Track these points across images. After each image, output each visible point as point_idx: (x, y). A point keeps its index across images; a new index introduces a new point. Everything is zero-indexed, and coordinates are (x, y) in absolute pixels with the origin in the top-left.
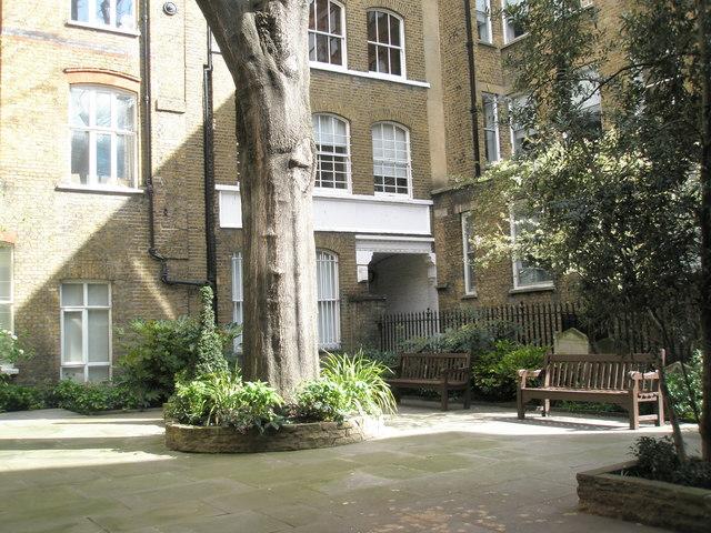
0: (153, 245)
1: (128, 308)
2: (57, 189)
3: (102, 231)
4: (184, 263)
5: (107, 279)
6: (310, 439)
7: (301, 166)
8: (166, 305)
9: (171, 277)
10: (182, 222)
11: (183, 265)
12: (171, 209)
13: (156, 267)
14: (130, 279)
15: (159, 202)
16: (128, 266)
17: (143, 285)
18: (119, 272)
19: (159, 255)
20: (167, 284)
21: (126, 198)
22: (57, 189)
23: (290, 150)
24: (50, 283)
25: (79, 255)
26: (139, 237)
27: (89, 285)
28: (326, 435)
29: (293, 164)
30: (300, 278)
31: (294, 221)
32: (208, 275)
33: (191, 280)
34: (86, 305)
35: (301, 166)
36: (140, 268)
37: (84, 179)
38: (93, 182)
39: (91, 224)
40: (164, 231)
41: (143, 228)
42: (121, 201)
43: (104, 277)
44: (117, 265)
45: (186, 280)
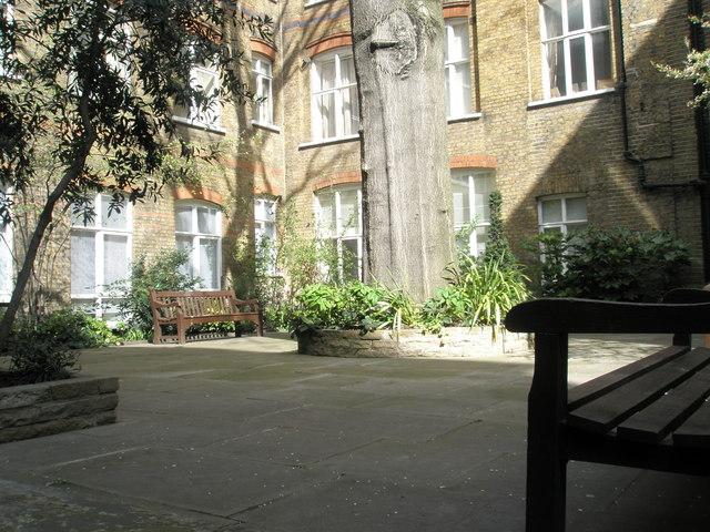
0: (627, 147)
1: (603, 220)
2: (530, 109)
3: (574, 141)
4: (667, 161)
5: (581, 191)
6: (332, 346)
7: (384, 46)
8: (647, 214)
9: (649, 181)
10: (664, 114)
11: (667, 165)
12: (649, 101)
13: (632, 171)
14: (604, 188)
15: (634, 96)
16: (602, 174)
17: (619, 193)
18: (592, 182)
19: (637, 157)
20: (649, 190)
21: (595, 101)
22: (530, 109)
23: (370, 33)
24: (525, 203)
25: (553, 170)
26: (613, 140)
27: (567, 200)
28: (346, 344)
29: (374, 47)
30: (391, 171)
31: (382, 109)
32: (701, 172)
33: (678, 181)
34: (564, 221)
35: (384, 46)
36: (617, 176)
37: (563, 92)
38: (571, 93)
39: (563, 136)
40: (641, 127)
41: (616, 131)
42: (588, 106)
43: (577, 190)
44: (590, 176)
45: (670, 181)
